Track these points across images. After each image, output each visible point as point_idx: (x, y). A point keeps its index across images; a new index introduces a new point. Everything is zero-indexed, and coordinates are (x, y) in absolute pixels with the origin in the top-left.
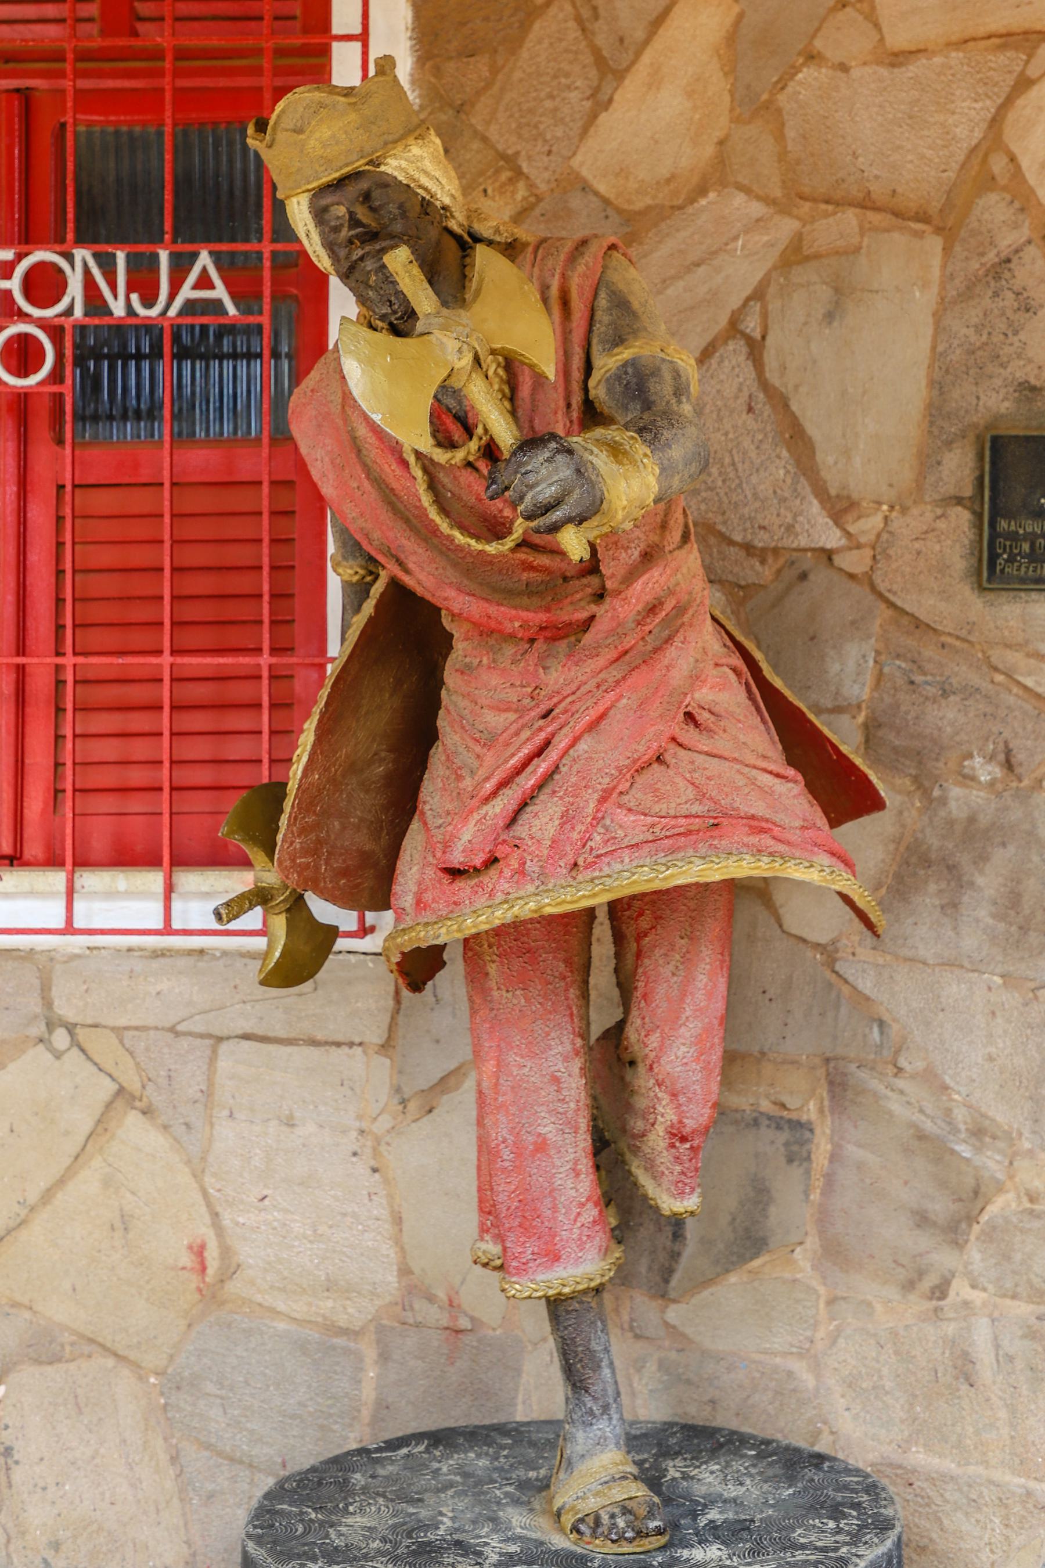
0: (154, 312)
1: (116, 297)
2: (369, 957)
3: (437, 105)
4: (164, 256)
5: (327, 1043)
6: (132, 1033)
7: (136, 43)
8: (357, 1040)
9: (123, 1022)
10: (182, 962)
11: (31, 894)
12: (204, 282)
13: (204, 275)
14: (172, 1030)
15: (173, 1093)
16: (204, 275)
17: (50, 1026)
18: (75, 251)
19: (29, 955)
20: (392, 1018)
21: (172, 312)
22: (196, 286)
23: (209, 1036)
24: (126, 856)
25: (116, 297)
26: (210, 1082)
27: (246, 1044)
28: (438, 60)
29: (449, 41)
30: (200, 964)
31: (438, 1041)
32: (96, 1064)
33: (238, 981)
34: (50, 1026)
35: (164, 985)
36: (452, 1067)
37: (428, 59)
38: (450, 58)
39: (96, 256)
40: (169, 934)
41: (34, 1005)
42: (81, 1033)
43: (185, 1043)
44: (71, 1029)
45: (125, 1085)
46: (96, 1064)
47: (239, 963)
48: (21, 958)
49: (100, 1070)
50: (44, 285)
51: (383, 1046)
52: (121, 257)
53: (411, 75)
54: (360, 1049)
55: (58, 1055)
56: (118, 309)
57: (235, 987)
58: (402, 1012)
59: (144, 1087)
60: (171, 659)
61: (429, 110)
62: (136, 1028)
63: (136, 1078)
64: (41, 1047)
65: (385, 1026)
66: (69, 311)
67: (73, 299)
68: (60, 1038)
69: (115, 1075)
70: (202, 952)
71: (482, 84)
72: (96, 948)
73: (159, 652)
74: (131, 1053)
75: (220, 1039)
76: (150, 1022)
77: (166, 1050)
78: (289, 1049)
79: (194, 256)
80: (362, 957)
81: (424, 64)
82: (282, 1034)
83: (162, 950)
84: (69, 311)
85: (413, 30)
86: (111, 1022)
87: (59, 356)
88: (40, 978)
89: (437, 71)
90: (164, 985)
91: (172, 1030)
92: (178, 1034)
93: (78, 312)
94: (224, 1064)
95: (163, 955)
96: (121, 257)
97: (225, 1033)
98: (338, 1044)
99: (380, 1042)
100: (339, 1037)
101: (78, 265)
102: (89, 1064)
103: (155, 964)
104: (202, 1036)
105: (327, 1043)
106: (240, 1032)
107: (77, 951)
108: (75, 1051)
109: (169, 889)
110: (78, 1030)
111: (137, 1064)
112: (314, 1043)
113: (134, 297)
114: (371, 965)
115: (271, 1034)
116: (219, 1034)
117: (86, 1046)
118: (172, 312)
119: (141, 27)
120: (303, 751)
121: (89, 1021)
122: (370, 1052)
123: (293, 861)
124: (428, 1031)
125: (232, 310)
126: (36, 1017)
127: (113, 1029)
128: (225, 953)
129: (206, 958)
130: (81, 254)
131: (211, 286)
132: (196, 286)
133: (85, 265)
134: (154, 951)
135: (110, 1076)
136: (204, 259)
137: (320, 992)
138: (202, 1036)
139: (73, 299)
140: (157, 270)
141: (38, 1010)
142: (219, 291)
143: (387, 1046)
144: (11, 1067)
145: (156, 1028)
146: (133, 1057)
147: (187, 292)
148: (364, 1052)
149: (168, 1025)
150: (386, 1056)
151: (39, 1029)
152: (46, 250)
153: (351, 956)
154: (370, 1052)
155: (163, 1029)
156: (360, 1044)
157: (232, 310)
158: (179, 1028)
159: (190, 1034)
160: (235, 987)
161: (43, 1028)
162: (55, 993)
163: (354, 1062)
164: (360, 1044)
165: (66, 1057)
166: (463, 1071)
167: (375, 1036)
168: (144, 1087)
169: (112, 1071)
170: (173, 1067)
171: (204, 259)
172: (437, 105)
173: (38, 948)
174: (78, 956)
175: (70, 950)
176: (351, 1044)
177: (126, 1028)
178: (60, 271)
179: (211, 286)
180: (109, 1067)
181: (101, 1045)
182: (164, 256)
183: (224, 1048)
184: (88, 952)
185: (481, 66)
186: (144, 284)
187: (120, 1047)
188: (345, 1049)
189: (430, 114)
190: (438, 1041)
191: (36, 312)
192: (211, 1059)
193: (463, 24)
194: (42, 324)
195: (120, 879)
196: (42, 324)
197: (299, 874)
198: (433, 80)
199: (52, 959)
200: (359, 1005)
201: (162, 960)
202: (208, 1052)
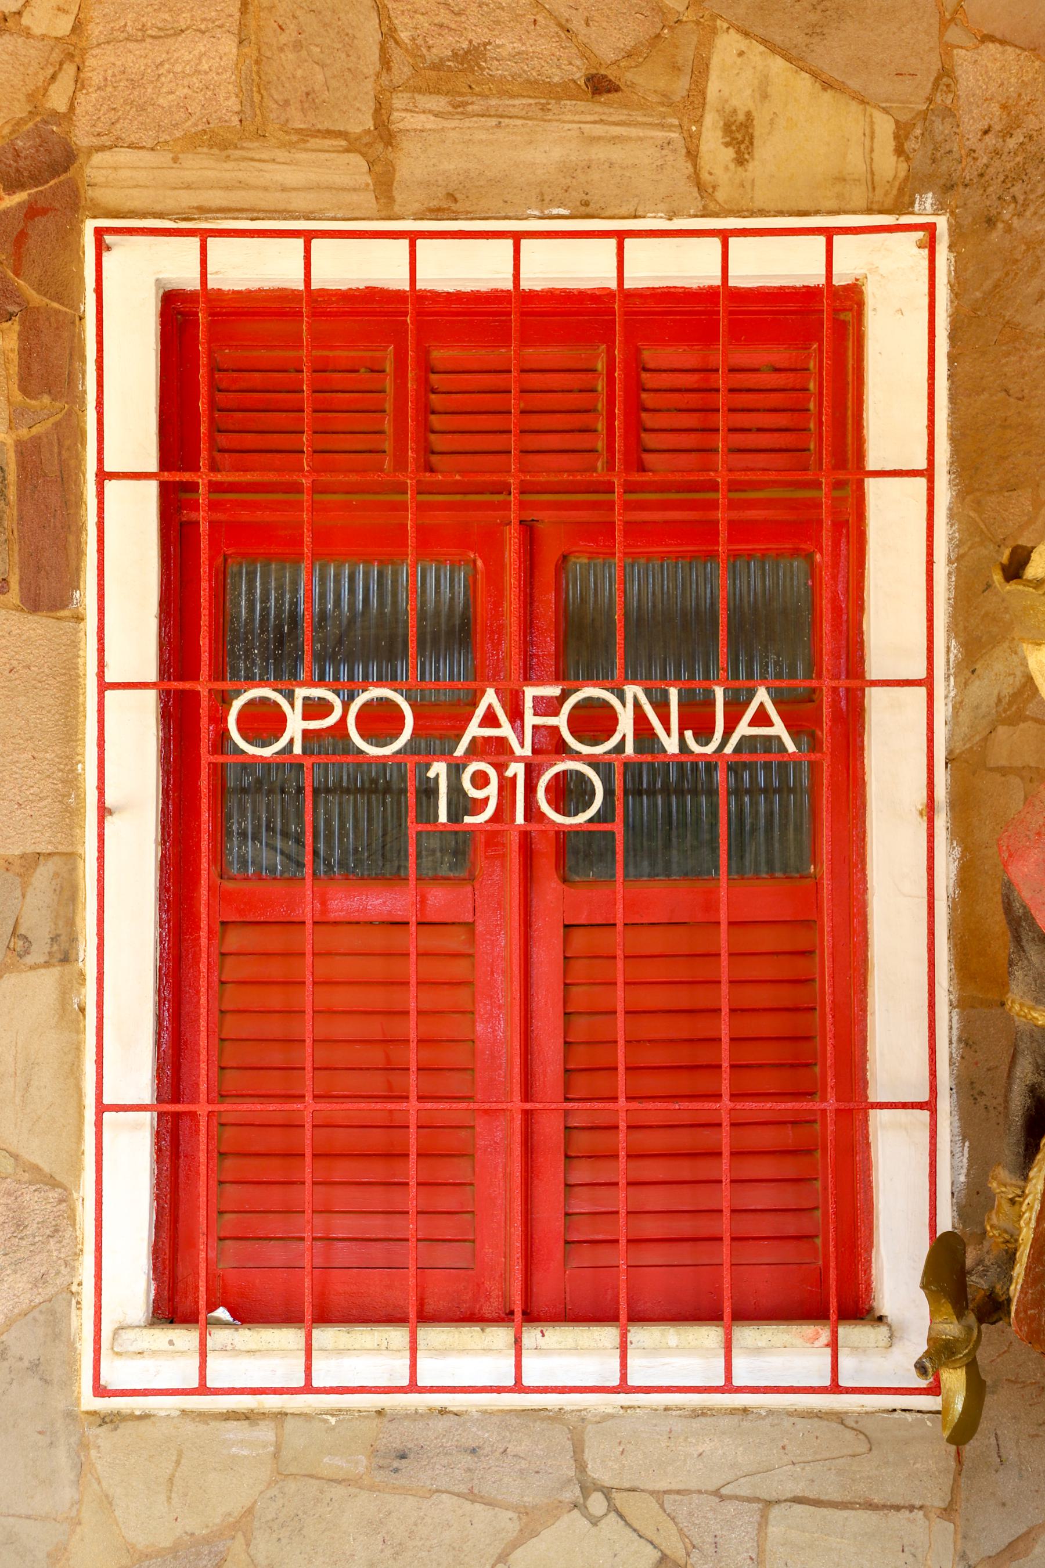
0: (710, 749)
1: (669, 734)
2: (926, 1416)
3: (977, 539)
4: (719, 693)
5: (884, 1507)
6: (672, 1497)
7: (647, 477)
8: (918, 1503)
9: (662, 1485)
10: (726, 1422)
11: (577, 1349)
12: (490, 719)
13: (762, 711)
14: (716, 1493)
15: (719, 1561)
16: (762, 711)
17: (586, 1490)
18: (525, 688)
19: (558, 1416)
20: (955, 1480)
21: (729, 749)
22: (752, 724)
23: (758, 1500)
24: (699, 1311)
25: (669, 734)
26: (761, 1550)
27: (798, 1508)
28: (978, 494)
29: (990, 476)
30: (745, 1424)
31: (1004, 1504)
32: (635, 1530)
33: (786, 1442)
34: (586, 1490)
35: (706, 1447)
36: (1021, 1532)
37: (968, 493)
38: (991, 492)
39: (648, 693)
40: (730, 1392)
41: (569, 1470)
42: (618, 1498)
43: (731, 1507)
44: (607, 1492)
45: (668, 1552)
46: (635, 1530)
47: (787, 1423)
48: (549, 1418)
49: (640, 1536)
50: (594, 722)
51: (945, 1510)
52: (673, 694)
53: (950, 509)
54: (921, 1513)
55: (595, 1522)
56: (671, 745)
57: (784, 1448)
58: (963, 1473)
59: (688, 1554)
60: (731, 1105)
61: (969, 543)
62: (678, 1492)
63: (680, 1545)
64: (576, 1513)
65: (947, 1489)
66: (620, 748)
67: (624, 736)
68: (597, 1503)
69: (656, 1542)
70: (745, 1410)
71: (1026, 518)
72: (630, 1407)
73: (717, 1096)
74: (673, 1519)
75: (769, 1503)
76: (693, 1485)
77: (710, 1515)
78: (846, 1513)
79: (751, 694)
80: (919, 1415)
81: (964, 499)
82: (836, 1497)
83: (702, 1409)
84: (620, 748)
85: (952, 464)
86: (650, 1487)
87: (609, 793)
88: (572, 1439)
89: (978, 505)
90: (706, 1447)
91: (716, 1493)
92: (722, 1498)
93: (629, 749)
94: (774, 1531)
95: (703, 1414)
96: (673, 694)
97: (774, 1496)
98: (898, 1508)
99: (943, 1505)
100: (900, 1501)
101: (628, 703)
102: (628, 1531)
103: (696, 1424)
104: (749, 1500)
105: (884, 1507)
106: (789, 1495)
107: (610, 1410)
108: (613, 1515)
109: (834, 1345)
110: (614, 1494)
111: (680, 1530)
112: (871, 1506)
113: (689, 734)
114: (929, 1424)
115: (823, 1498)
116: (767, 1497)
117: (625, 1512)
118: (729, 749)
119: (649, 458)
120: (1035, 1200)
121: (627, 1485)
122: (932, 1515)
123: (1026, 1312)
124: (993, 1494)
125: (791, 747)
126: (570, 1481)
127: (652, 1493)
128: (771, 1412)
129: (750, 1417)
130: (632, 691)
131: (770, 724)
132: (752, 724)
133: (635, 698)
134: (694, 1410)
135: (652, 1543)
136: (762, 696)
137: (875, 1452)
138: (749, 1500)
139: (624, 736)
140: (713, 704)
141: (572, 1473)
142: (778, 729)
143: (948, 1511)
144: (545, 1534)
145: (700, 1492)
146: (676, 1524)
147: (743, 729)
148: (926, 1516)
149: (713, 1489)
150: (950, 1521)
151: (573, 1493)
152: (594, 686)
153: (907, 1415)
154: (932, 1515)
155: (706, 1492)
156: (921, 1508)
157: (791, 747)
158: (723, 1491)
159: (736, 1498)
160: (784, 1448)
161: (577, 1491)
162: (588, 1455)
163: (914, 1527)
164: (921, 1508)
165: (602, 1524)
166: (1032, 1535)
167: (937, 1500)
168: (688, 1554)
169: (654, 1538)
170: (718, 1533)
171: (762, 696)
172: (977, 539)
173: (567, 1408)
174: (612, 1416)
175: (602, 1409)
176: (911, 1508)
177: (665, 1492)
178: (611, 708)
179: (770, 724)
180: (650, 1533)
181: (637, 1507)
182: (719, 693)
183: (775, 1512)
184: (622, 1412)
185: (1023, 499)
186: (698, 721)
187: (661, 1511)
188: (905, 1514)
189: (970, 548)
190: (1004, 1504)
191: (585, 750)
192: (760, 1524)
193: (1002, 458)
194: (593, 762)
195: (469, 1335)
196: (593, 762)
197: (1029, 1325)
198: (972, 514)
199: (583, 1420)
200: (918, 1465)
201: (703, 1419)
202: (757, 1517)
